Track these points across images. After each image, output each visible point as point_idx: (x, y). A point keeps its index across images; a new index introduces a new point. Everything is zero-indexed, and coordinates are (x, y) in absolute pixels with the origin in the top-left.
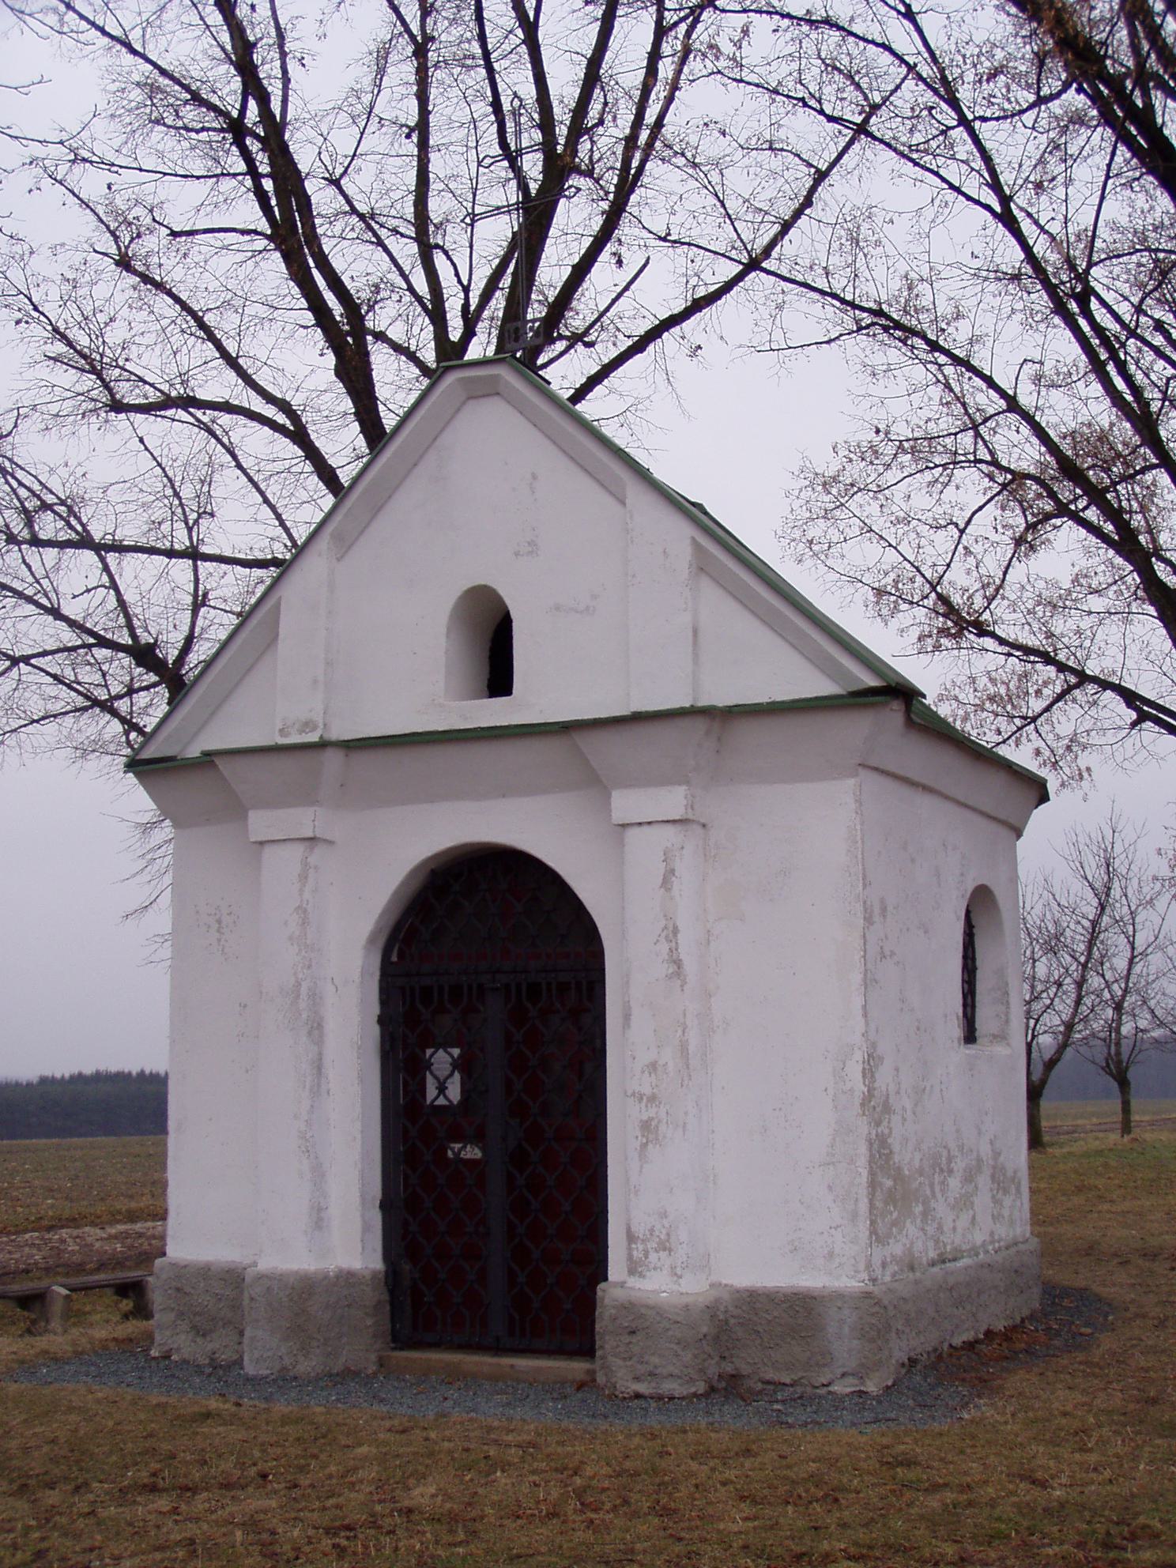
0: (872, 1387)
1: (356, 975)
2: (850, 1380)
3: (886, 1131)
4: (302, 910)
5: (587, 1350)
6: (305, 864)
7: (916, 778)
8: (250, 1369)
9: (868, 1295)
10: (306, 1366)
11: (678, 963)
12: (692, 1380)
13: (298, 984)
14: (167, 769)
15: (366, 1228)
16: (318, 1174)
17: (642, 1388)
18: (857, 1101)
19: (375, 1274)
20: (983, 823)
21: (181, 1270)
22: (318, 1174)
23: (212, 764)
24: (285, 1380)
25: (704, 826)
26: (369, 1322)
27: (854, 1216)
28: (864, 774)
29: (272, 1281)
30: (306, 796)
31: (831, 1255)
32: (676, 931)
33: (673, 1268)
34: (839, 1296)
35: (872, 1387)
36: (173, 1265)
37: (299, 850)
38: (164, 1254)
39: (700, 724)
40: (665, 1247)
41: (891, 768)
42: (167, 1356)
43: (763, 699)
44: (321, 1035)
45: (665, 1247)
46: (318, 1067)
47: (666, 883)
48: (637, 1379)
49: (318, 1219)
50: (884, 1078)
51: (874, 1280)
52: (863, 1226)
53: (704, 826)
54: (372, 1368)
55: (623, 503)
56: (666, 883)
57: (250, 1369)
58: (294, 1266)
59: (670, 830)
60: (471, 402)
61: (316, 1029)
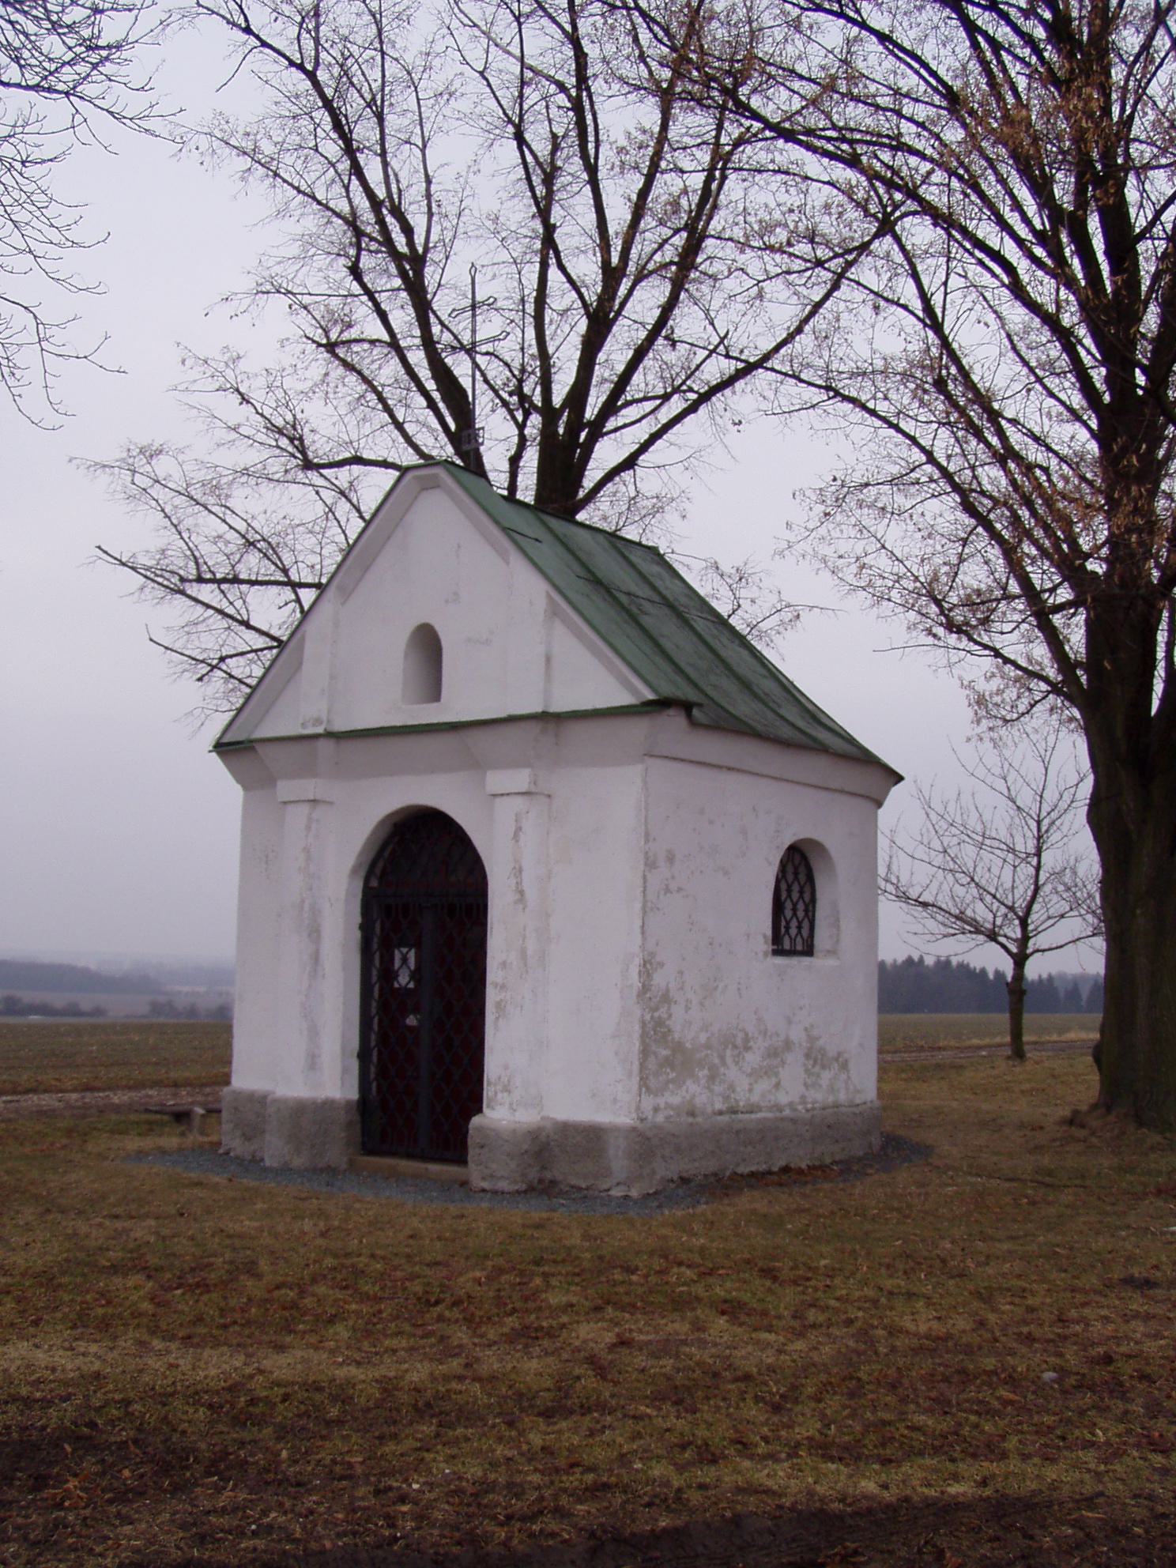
0: (634, 1193)
1: (342, 894)
2: (622, 1188)
3: (665, 1016)
4: (307, 850)
5: (462, 1160)
6: (310, 819)
7: (714, 762)
8: (268, 1163)
9: (634, 1129)
10: (298, 1162)
11: (522, 893)
12: (515, 1182)
13: (303, 901)
14: (236, 750)
15: (345, 1070)
16: (313, 1032)
17: (485, 1185)
18: (635, 993)
19: (349, 1103)
20: (844, 799)
21: (238, 1095)
22: (313, 1032)
23: (253, 748)
24: (285, 1170)
25: (549, 796)
26: (343, 1135)
27: (630, 1074)
28: (650, 761)
29: (283, 1102)
30: (307, 770)
31: (615, 1100)
32: (521, 870)
33: (511, 1104)
34: (615, 1129)
35: (634, 1193)
36: (234, 1092)
37: (305, 809)
38: (228, 1082)
39: (534, 728)
40: (507, 1089)
41: (680, 755)
42: (227, 1153)
43: (589, 707)
44: (319, 936)
45: (507, 1089)
46: (316, 958)
47: (516, 836)
48: (484, 1178)
49: (313, 1062)
50: (659, 979)
51: (642, 1120)
52: (636, 1079)
53: (549, 796)
54: (344, 1166)
55: (508, 563)
56: (516, 836)
57: (268, 1163)
58: (295, 1094)
59: (519, 800)
60: (425, 494)
61: (315, 933)
